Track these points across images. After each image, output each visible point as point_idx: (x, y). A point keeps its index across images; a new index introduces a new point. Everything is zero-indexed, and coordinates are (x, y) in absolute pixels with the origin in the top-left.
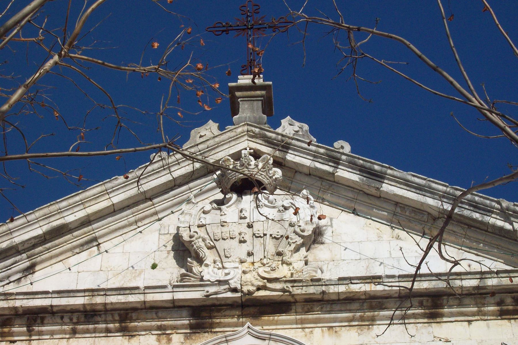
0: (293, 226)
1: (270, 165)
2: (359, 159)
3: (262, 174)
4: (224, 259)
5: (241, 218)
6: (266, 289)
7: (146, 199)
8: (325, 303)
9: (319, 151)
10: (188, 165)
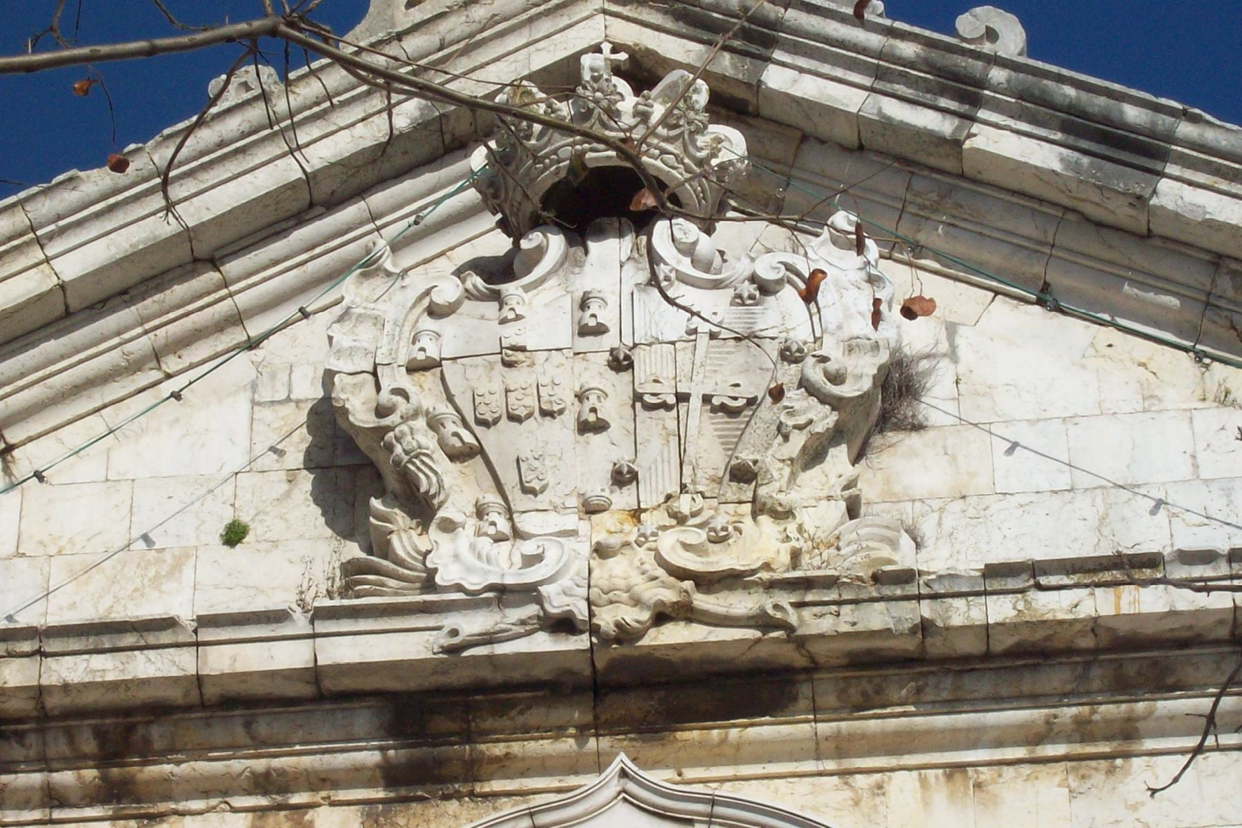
2: (1060, 79)
4: (520, 501)
5: (584, 331)
7: (196, 260)
8: (934, 669)
9: (898, 52)
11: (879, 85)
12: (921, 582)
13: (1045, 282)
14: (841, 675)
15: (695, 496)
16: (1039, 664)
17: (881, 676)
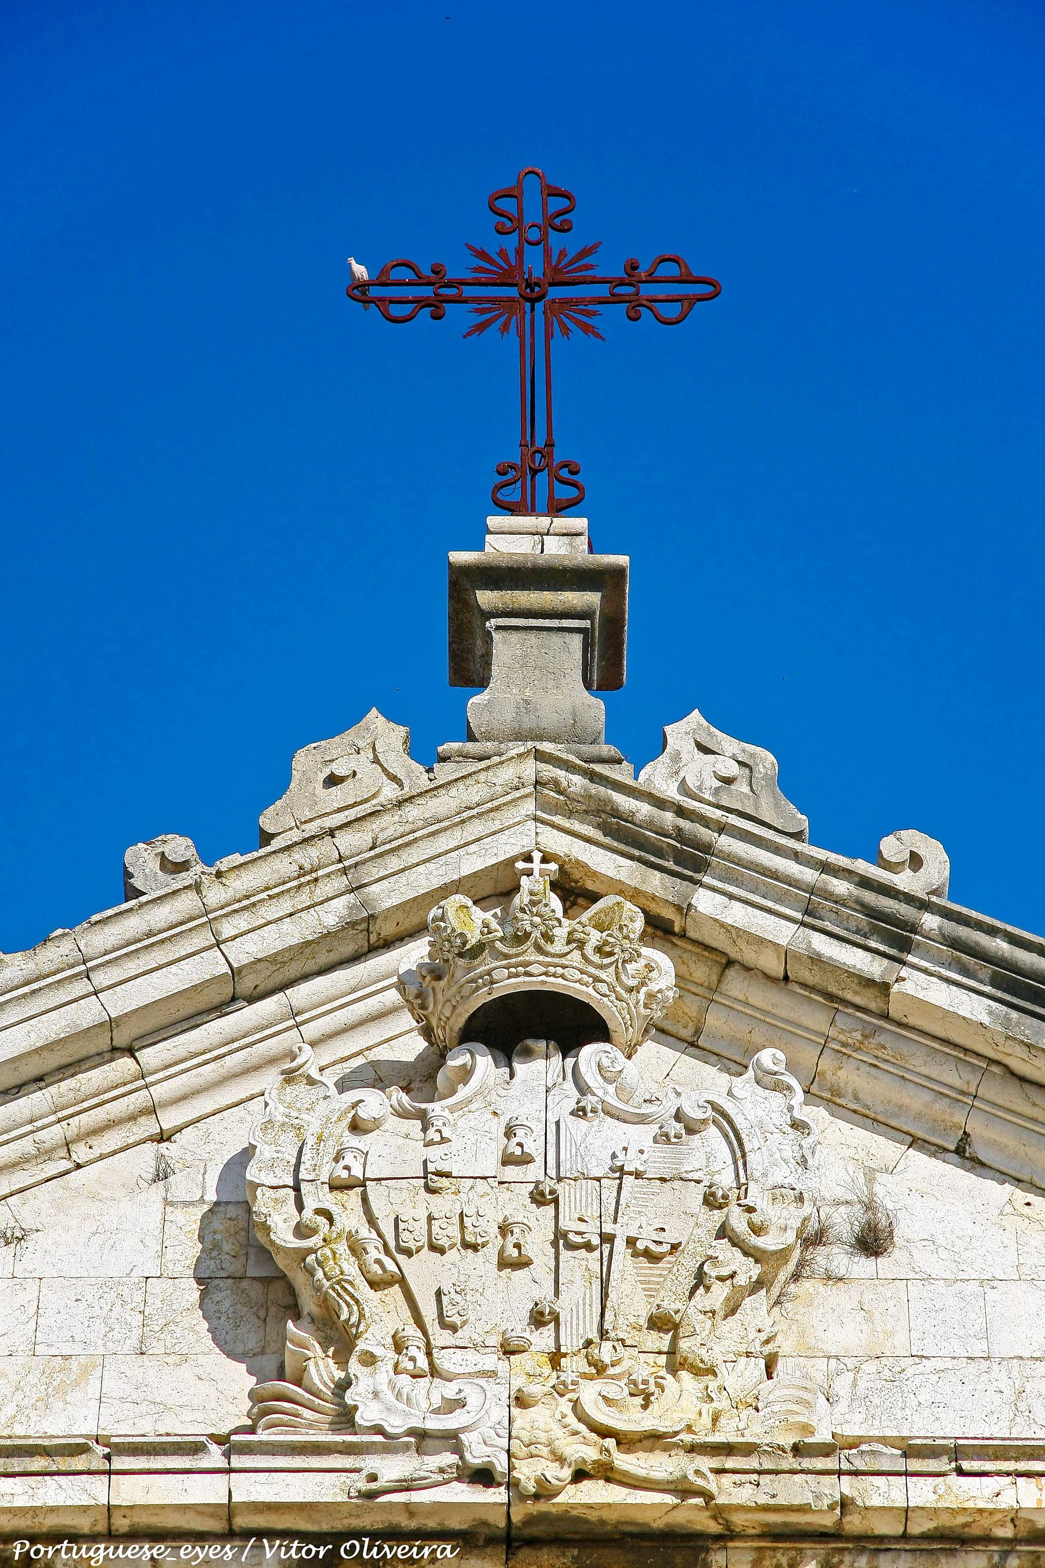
0: (720, 1207)
1: (631, 941)
2: (992, 931)
3: (597, 980)
4: (440, 1337)
5: (507, 1160)
6: (609, 1474)
7: (114, 1049)
8: (850, 1546)
9: (830, 888)
10: (291, 915)
11: (807, 919)
12: (842, 1456)
13: (965, 1132)
14: (755, 1544)
15: (615, 1344)
16: (955, 1549)
17: (796, 1549)
